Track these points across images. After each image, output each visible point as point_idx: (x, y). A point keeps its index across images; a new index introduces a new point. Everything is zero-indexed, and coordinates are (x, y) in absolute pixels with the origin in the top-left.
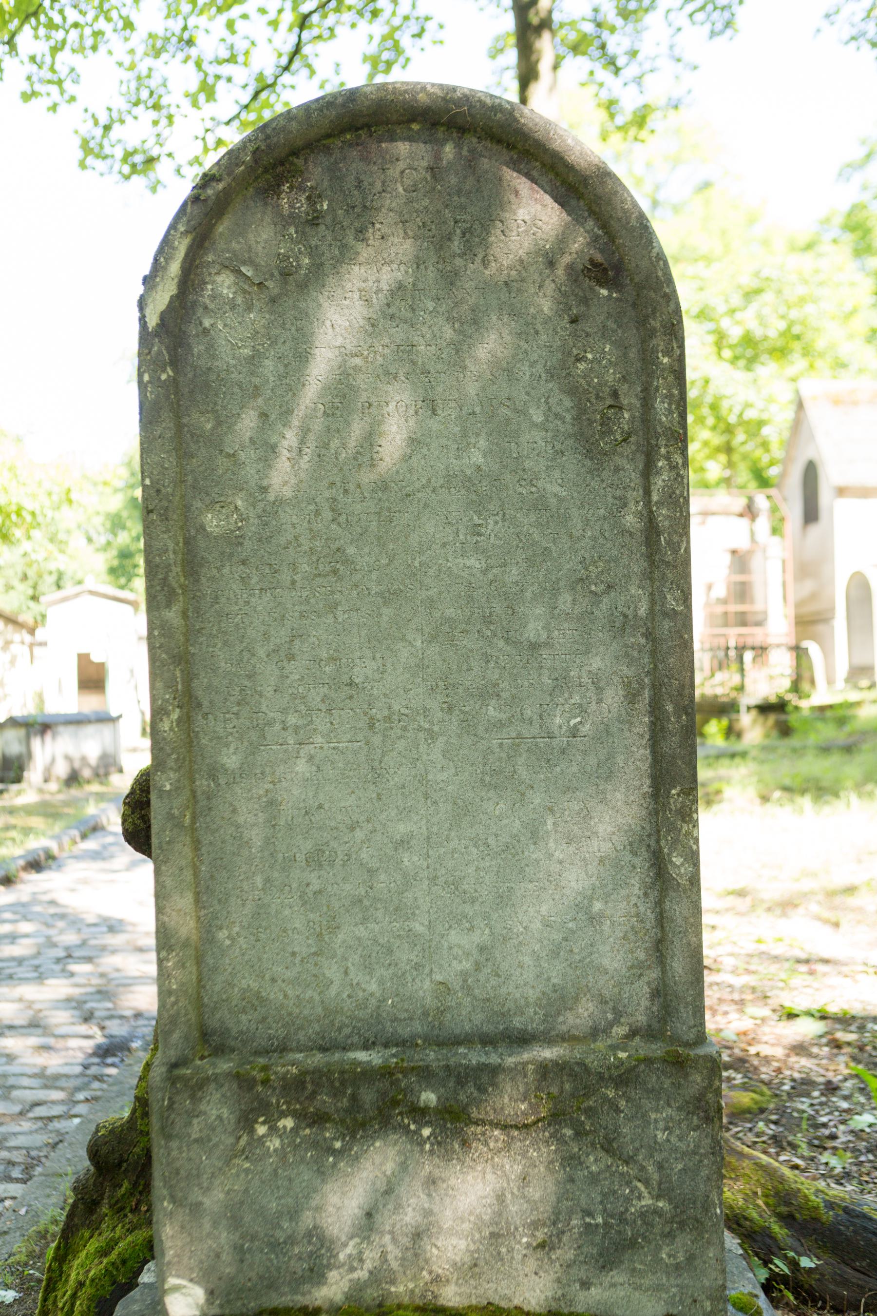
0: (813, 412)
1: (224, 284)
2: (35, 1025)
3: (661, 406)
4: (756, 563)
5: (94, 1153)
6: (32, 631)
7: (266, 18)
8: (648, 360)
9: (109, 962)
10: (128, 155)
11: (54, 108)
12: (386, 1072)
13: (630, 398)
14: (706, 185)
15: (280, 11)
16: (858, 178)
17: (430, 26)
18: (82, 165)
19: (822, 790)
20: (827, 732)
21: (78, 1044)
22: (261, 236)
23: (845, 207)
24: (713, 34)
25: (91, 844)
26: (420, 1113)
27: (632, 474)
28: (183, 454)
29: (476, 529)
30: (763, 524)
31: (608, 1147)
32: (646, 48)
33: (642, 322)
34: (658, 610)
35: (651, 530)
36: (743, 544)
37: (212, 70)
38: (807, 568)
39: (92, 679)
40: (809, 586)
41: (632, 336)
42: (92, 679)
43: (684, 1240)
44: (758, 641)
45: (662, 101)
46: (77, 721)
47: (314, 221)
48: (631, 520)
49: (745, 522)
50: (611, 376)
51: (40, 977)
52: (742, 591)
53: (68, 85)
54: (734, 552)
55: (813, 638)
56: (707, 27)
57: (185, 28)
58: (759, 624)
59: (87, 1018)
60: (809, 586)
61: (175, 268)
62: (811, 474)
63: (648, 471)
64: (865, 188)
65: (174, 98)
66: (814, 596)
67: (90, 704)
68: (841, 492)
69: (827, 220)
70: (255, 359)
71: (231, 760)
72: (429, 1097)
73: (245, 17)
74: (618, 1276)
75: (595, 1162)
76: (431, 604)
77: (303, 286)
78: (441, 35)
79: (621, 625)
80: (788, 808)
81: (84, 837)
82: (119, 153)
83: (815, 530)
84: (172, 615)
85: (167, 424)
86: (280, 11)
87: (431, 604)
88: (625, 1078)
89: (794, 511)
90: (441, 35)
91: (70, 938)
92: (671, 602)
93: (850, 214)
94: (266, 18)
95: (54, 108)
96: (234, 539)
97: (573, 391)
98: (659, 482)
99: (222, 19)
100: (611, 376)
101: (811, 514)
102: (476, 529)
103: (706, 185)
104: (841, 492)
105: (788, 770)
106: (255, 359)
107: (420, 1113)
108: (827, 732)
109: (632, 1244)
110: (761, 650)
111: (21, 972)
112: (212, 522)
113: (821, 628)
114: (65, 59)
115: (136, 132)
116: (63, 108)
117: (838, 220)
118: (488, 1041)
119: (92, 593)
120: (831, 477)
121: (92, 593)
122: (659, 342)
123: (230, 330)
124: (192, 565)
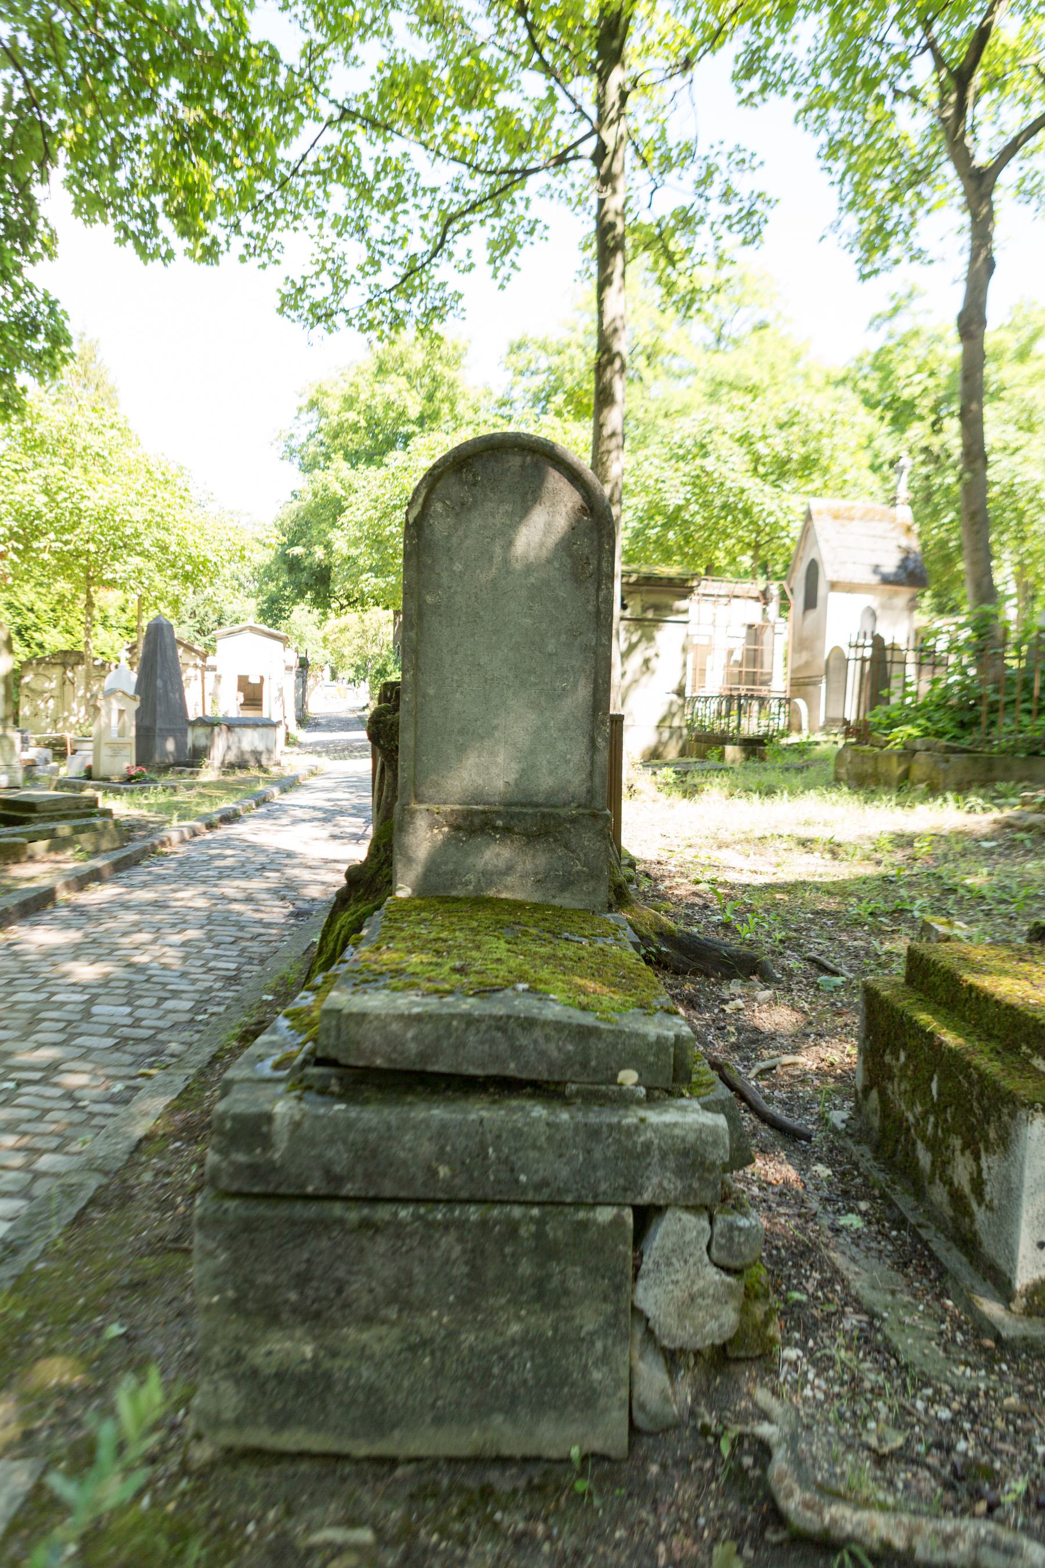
0: (818, 523)
1: (438, 507)
2: (249, 899)
3: (604, 564)
4: (767, 636)
5: (349, 875)
6: (204, 657)
7: (419, 213)
8: (600, 545)
9: (291, 872)
10: (314, 306)
11: (264, 266)
12: (483, 812)
13: (594, 562)
14: (762, 326)
15: (430, 208)
16: (886, 327)
17: (539, 227)
18: (281, 311)
19: (769, 791)
20: (794, 759)
21: (277, 912)
22: (454, 489)
23: (874, 349)
24: (745, 243)
25: (262, 810)
26: (496, 829)
27: (592, 590)
28: (419, 572)
29: (530, 608)
30: (773, 607)
31: (566, 846)
32: (698, 247)
33: (599, 531)
34: (599, 643)
35: (598, 612)
36: (757, 620)
37: (380, 247)
38: (803, 643)
39: (252, 697)
40: (805, 656)
41: (595, 535)
42: (252, 697)
43: (592, 883)
44: (763, 694)
45: (706, 287)
46: (244, 724)
47: (475, 484)
48: (590, 608)
49: (759, 606)
50: (587, 551)
51: (248, 877)
52: (754, 657)
53: (275, 253)
54: (750, 626)
55: (804, 697)
56: (741, 236)
57: (361, 217)
58: (764, 683)
59: (283, 899)
60: (805, 656)
61: (421, 500)
62: (813, 569)
63: (598, 589)
64: (890, 337)
65: (350, 269)
66: (807, 664)
67: (250, 714)
68: (833, 586)
69: (861, 359)
70: (448, 537)
71: (431, 691)
72: (499, 823)
73: (405, 212)
74: (567, 895)
75: (561, 851)
76: (512, 636)
77: (469, 509)
78: (546, 234)
79: (585, 648)
80: (744, 800)
81: (258, 805)
82: (307, 304)
83: (812, 614)
84: (412, 634)
85: (414, 561)
86: (430, 208)
87: (512, 636)
88: (573, 820)
89: (797, 601)
90: (546, 234)
91: (262, 859)
92: (604, 641)
93: (877, 357)
94: (419, 213)
95: (264, 266)
96: (437, 606)
97: (571, 556)
98: (602, 594)
99: (389, 214)
100: (587, 551)
101: (811, 602)
102: (530, 608)
103: (762, 326)
104: (833, 586)
105: (753, 780)
106: (448, 537)
107: (496, 829)
108: (794, 759)
109: (572, 883)
110: (762, 701)
111: (234, 874)
112: (429, 599)
113: (811, 688)
114: (274, 235)
115: (321, 291)
116: (271, 267)
117: (869, 359)
118: (523, 805)
119: (252, 629)
120: (828, 573)
121: (252, 629)
122: (605, 539)
123: (440, 526)
124: (421, 615)
